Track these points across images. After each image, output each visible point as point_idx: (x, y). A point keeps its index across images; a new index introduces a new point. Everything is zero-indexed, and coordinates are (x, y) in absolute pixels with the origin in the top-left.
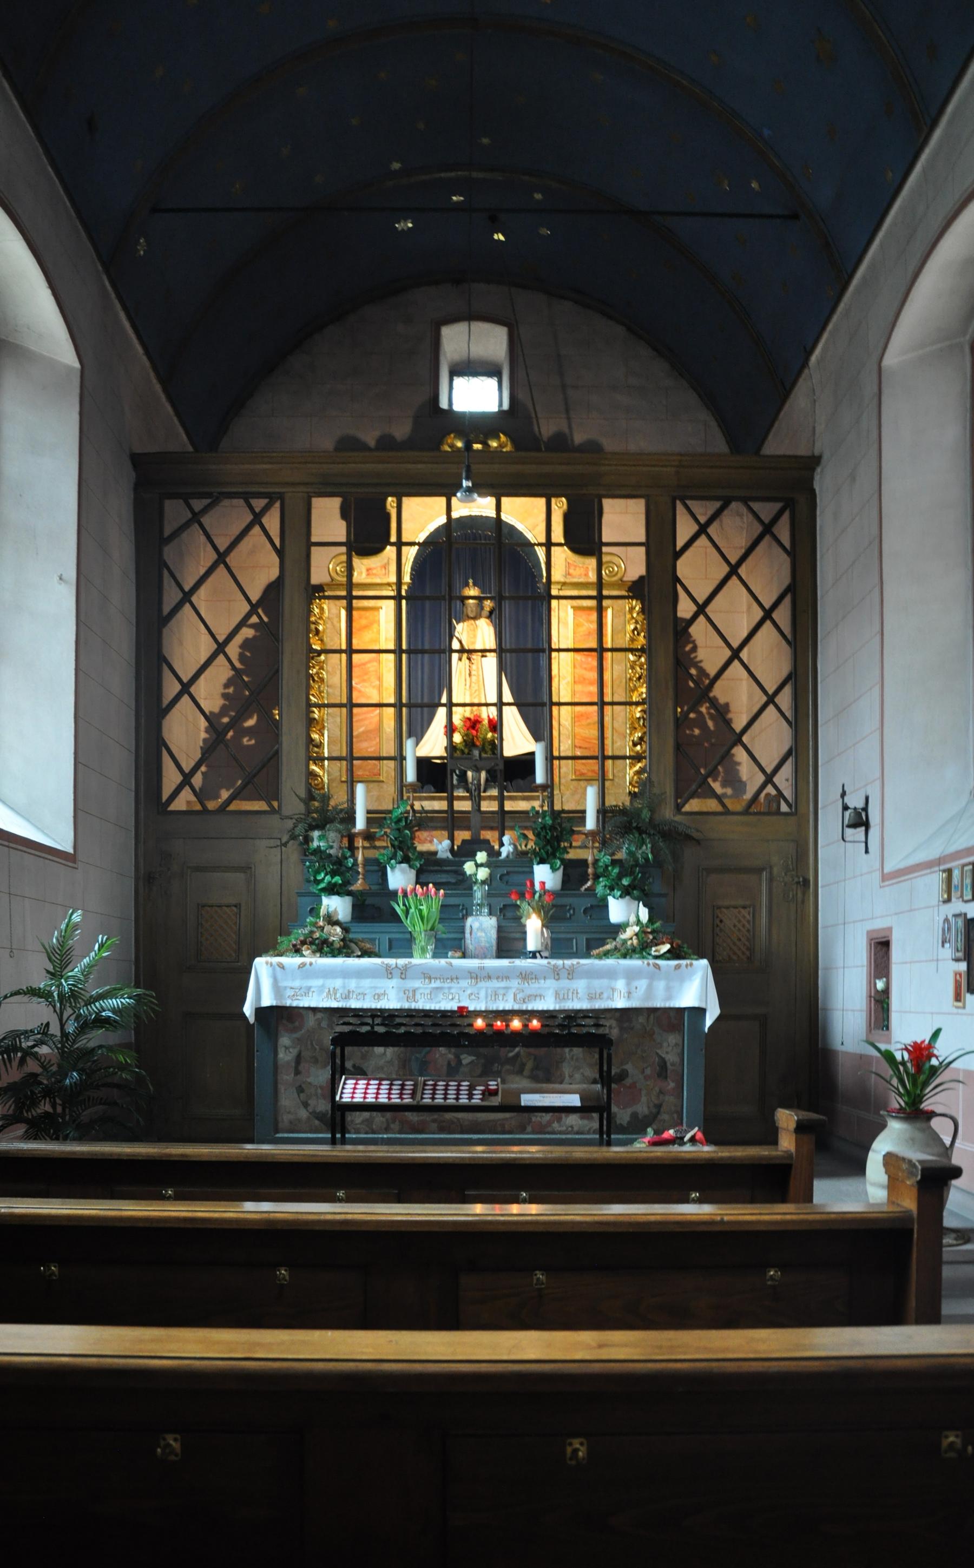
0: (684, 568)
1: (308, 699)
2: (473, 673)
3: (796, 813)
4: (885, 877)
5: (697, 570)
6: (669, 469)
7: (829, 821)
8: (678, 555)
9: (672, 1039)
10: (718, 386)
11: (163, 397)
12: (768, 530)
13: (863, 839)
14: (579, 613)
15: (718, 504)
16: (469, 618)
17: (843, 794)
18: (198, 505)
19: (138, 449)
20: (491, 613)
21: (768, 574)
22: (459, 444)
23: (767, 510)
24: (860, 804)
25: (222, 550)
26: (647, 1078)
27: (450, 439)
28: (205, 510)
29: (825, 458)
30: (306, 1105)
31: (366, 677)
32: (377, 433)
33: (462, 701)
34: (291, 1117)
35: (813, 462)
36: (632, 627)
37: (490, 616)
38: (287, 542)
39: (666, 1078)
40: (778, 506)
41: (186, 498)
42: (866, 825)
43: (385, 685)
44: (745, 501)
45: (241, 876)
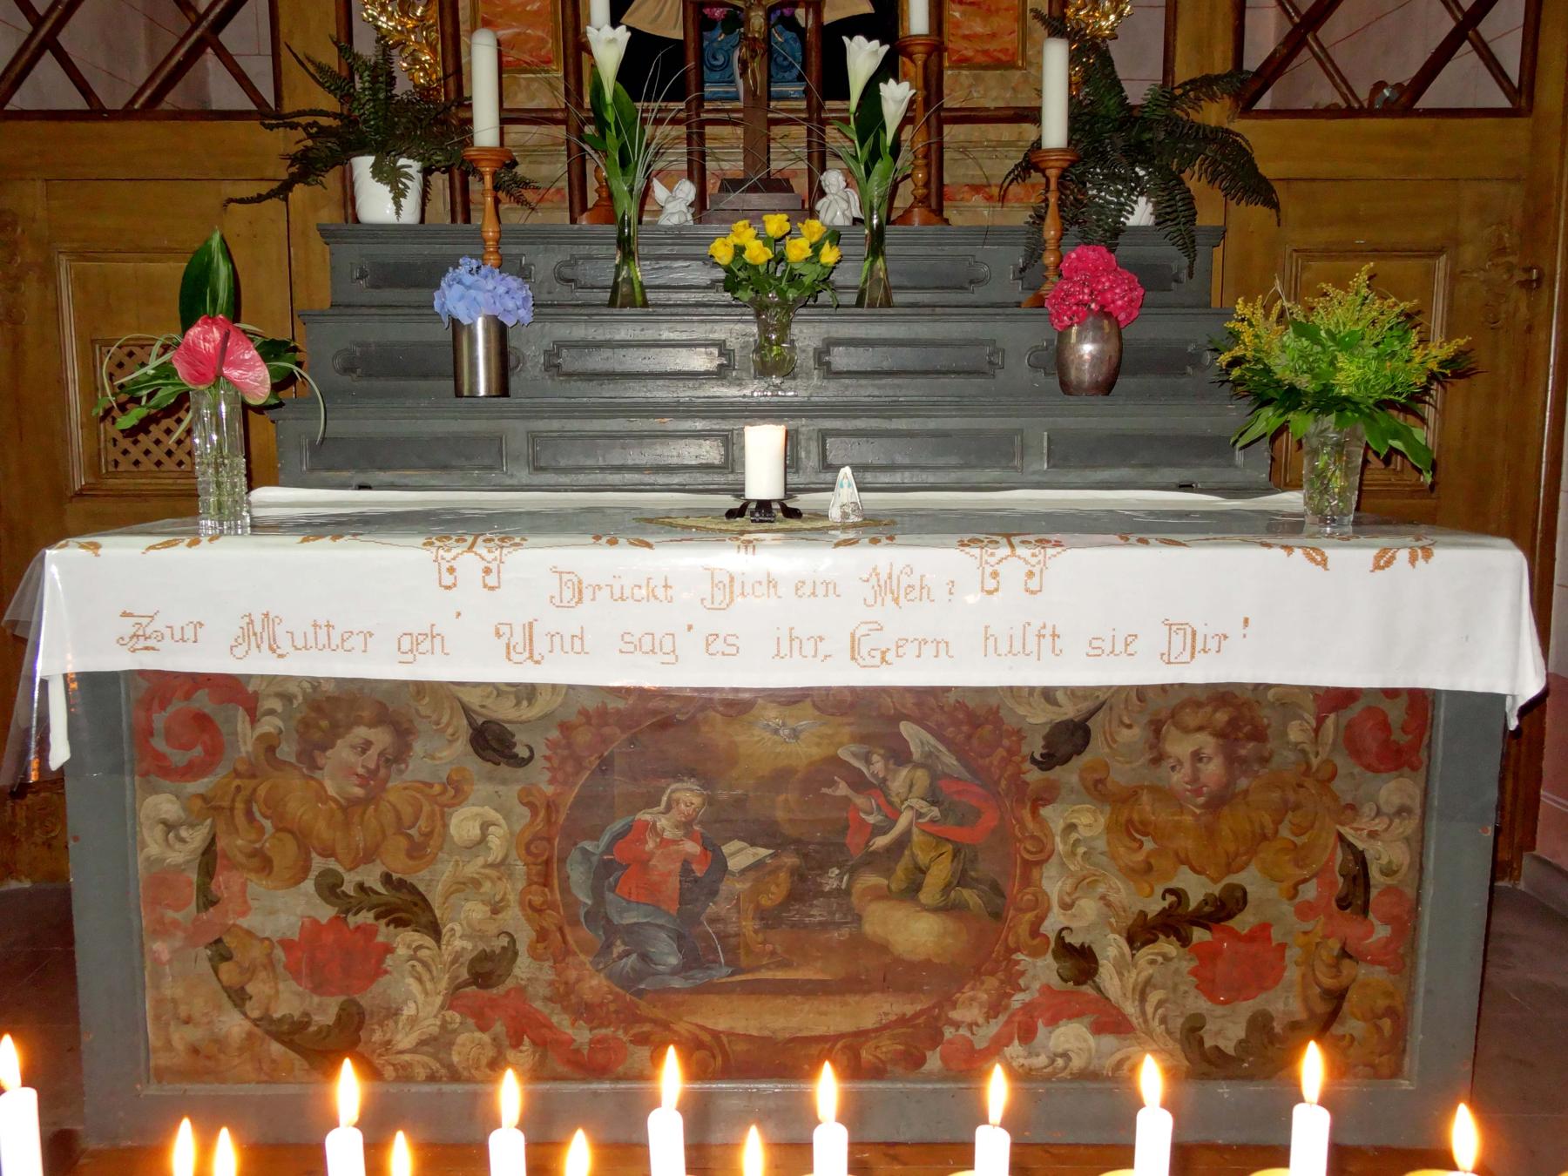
9: (1393, 790)
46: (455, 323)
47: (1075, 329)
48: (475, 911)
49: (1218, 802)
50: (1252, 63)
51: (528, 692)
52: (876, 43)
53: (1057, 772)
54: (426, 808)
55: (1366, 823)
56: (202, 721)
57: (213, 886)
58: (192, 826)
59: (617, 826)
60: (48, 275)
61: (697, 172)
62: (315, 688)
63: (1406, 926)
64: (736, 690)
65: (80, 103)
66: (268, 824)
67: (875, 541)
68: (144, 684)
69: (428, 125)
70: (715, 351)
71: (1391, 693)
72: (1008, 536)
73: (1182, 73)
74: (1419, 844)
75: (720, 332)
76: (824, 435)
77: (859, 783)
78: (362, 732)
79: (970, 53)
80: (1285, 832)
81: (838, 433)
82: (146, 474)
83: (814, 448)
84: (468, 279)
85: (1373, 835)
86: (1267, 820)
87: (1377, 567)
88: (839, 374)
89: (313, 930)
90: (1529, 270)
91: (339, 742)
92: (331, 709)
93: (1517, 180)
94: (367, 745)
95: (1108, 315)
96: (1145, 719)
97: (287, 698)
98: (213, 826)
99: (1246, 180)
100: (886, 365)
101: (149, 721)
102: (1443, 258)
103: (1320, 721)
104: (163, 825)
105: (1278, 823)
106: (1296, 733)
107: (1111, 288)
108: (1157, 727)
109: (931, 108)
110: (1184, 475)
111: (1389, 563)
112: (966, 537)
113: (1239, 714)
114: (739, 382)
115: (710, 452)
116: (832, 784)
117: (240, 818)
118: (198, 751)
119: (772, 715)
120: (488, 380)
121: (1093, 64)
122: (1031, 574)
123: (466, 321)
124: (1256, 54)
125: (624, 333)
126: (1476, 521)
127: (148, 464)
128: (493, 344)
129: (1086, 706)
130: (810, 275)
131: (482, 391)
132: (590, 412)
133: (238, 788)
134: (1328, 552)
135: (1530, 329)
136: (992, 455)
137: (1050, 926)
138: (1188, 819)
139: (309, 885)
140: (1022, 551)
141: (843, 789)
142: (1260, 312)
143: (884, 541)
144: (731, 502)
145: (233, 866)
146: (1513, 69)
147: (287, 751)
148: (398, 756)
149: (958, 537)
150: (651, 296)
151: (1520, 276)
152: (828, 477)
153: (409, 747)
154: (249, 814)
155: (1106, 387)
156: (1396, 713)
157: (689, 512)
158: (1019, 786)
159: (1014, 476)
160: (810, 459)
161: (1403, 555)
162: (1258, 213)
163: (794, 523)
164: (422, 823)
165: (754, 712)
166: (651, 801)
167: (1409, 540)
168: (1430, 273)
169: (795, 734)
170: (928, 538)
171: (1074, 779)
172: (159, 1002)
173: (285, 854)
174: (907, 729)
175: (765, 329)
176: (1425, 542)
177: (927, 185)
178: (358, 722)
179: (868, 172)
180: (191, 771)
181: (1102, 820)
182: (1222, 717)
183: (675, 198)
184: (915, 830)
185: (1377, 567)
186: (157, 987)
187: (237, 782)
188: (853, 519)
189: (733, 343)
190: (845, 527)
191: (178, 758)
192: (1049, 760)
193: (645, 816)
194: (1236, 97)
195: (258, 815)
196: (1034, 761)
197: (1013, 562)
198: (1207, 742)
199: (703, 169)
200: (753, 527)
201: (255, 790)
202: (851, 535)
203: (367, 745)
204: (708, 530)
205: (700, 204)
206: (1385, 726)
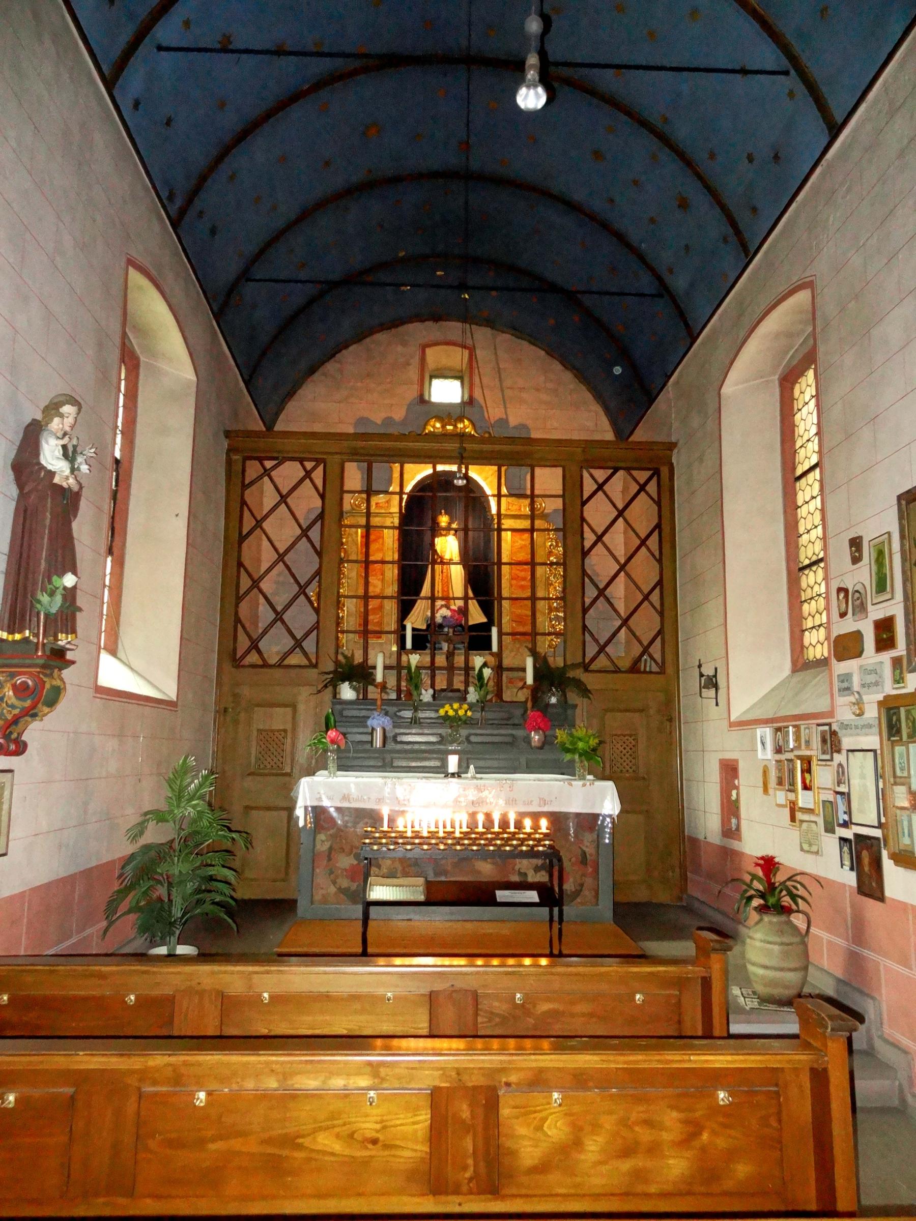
0: (589, 511)
1: (338, 592)
4: (731, 725)
5: (598, 513)
7: (689, 682)
8: (584, 503)
11: (245, 391)
12: (642, 488)
13: (714, 696)
15: (610, 471)
17: (700, 666)
18: (269, 464)
19: (228, 429)
21: (643, 513)
22: (438, 425)
23: (642, 476)
24: (712, 673)
25: (281, 551)
26: (573, 865)
27: (432, 422)
28: (274, 467)
30: (334, 883)
32: (383, 415)
34: (324, 892)
35: (672, 446)
39: (586, 864)
40: (650, 473)
41: (261, 460)
42: (716, 686)
43: (386, 578)
44: (628, 469)
48: (389, 862)
61: (433, 686)
63: (596, 870)
65: (260, 662)
69: (360, 674)
73: (569, 663)
75: (440, 731)
78: (366, 820)
89: (352, 866)
99: (585, 691)
109: (499, 669)
115: (438, 764)
126: (102, 687)
130: (464, 718)
135: (671, 733)
137: (517, 868)
155: (541, 748)
160: (464, 765)
189: (444, 734)
205: (434, 696)
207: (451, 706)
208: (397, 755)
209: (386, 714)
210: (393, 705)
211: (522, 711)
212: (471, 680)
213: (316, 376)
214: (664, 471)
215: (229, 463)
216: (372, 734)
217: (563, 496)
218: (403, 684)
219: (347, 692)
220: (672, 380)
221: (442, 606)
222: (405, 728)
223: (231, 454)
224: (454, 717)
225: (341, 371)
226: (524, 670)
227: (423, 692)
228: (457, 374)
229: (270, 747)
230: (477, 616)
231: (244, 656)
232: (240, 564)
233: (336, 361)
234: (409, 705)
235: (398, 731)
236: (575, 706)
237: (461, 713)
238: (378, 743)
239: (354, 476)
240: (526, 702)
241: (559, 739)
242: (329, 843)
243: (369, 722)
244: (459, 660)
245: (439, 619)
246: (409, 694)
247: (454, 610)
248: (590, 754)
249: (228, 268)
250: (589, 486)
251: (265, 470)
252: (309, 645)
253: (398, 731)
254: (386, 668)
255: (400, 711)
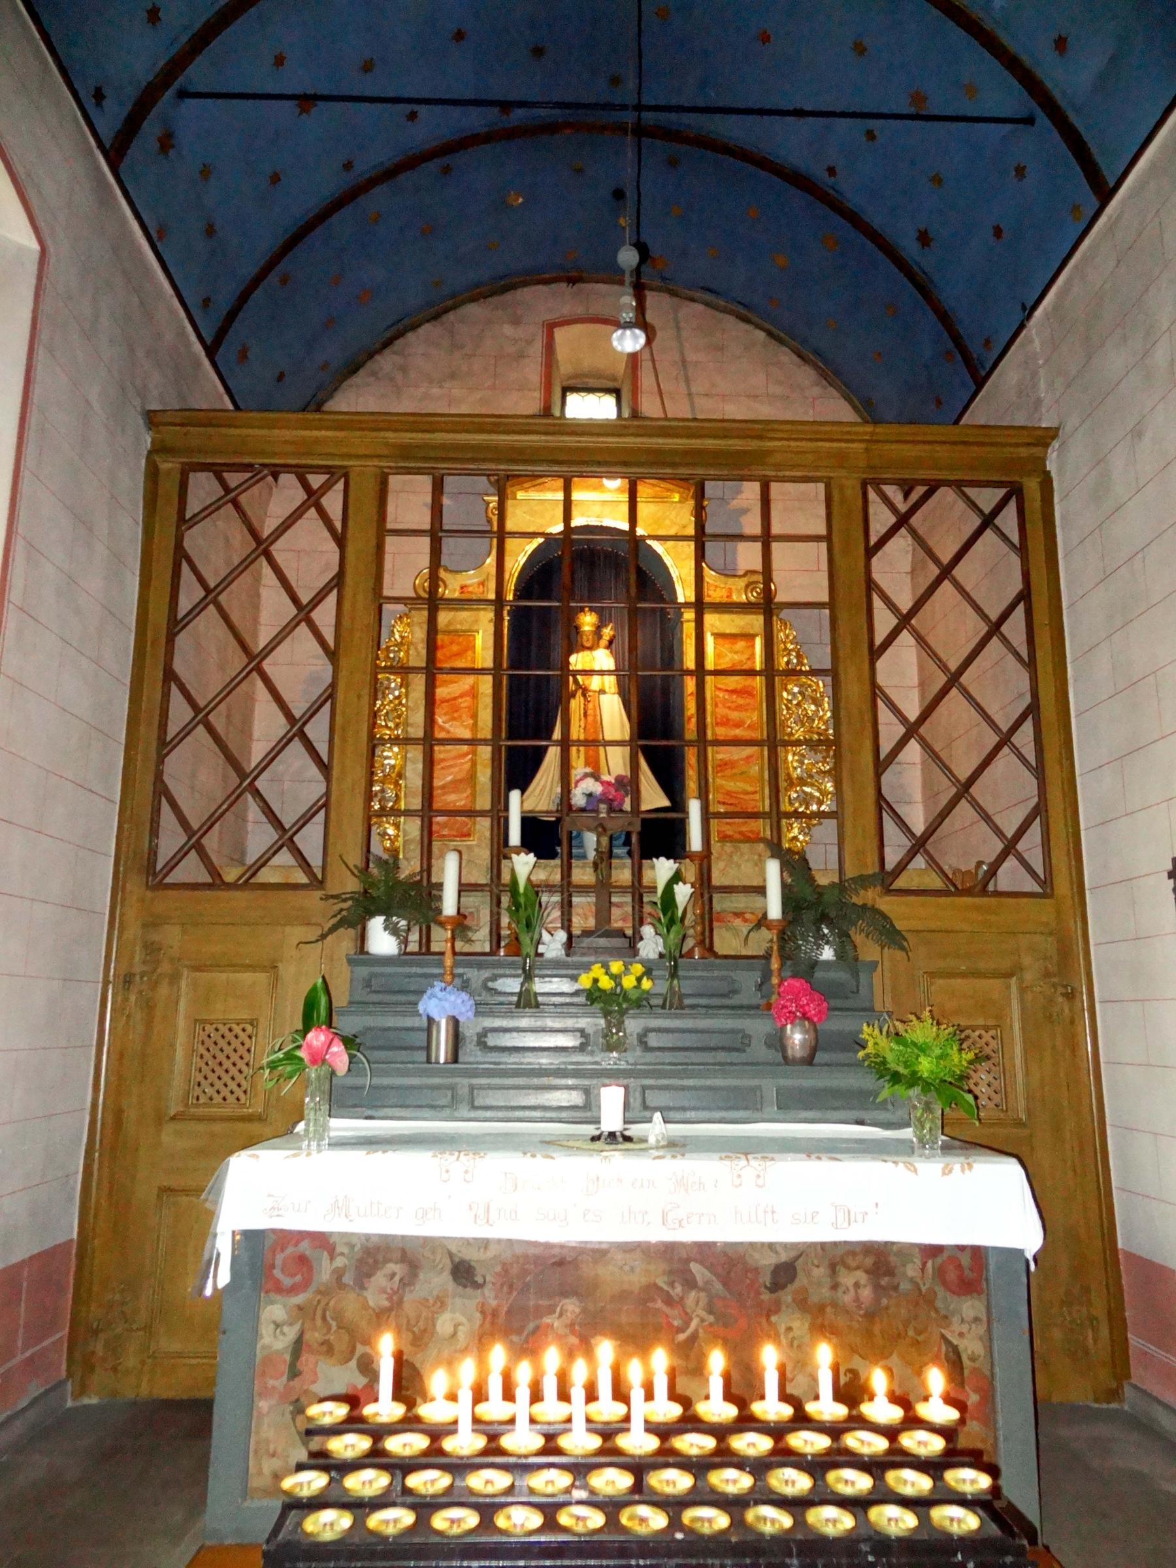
2: (590, 712)
3: (1051, 896)
6: (855, 445)
8: (871, 552)
9: (970, 1307)
10: (919, 344)
12: (988, 521)
14: (720, 641)
16: (584, 648)
20: (611, 642)
21: (992, 572)
23: (987, 498)
28: (244, 487)
29: (1068, 428)
31: (456, 715)
33: (776, 564)
35: (1046, 437)
36: (785, 659)
37: (610, 645)
38: (351, 523)
40: (1001, 492)
41: (217, 471)
43: (480, 723)
44: (958, 485)
45: (262, 977)
46: (430, 1020)
47: (789, 1027)
49: (870, 1316)
50: (889, 866)
51: (485, 1243)
52: (672, 861)
53: (781, 1293)
54: (424, 1314)
55: (956, 1326)
56: (303, 1260)
57: (298, 1364)
58: (291, 1324)
59: (531, 1326)
60: (175, 978)
61: (567, 925)
62: (367, 1241)
64: (600, 1243)
65: (206, 878)
66: (334, 1324)
67: (674, 1157)
68: (273, 1237)
69: (413, 900)
70: (578, 1034)
71: (962, 1248)
72: (746, 1154)
73: (850, 873)
74: (988, 1339)
75: (582, 1023)
76: (644, 1089)
77: (669, 1301)
79: (730, 833)
80: (911, 1333)
81: (651, 1088)
82: (218, 1106)
83: (638, 1095)
84: (440, 995)
85: (961, 1335)
86: (901, 1327)
87: (944, 1174)
88: (652, 1049)
90: (1065, 987)
91: (378, 1273)
92: (374, 1254)
93: (1051, 934)
94: (393, 1275)
95: (808, 1019)
96: (826, 1263)
97: (352, 1246)
98: (303, 1324)
99: (891, 936)
100: (680, 1044)
101: (274, 1259)
102: (1014, 978)
103: (924, 1264)
104: (275, 1325)
105: (906, 1327)
106: (912, 1271)
107: (808, 1004)
108: (833, 1268)
109: (705, 887)
110: (856, 1114)
111: (950, 1172)
112: (723, 1155)
113: (879, 1260)
114: (592, 1053)
115: (576, 1098)
116: (654, 1300)
117: (319, 1322)
118: (298, 1278)
119: (619, 1256)
120: (446, 1053)
121: (796, 865)
122: (758, 1176)
123: (437, 1019)
124: (892, 858)
125: (524, 1022)
127: (218, 1099)
128: (451, 1028)
129: (793, 1254)
130: (634, 995)
131: (442, 1060)
132: (504, 1073)
133: (319, 1302)
134: (916, 1165)
135: (1072, 1022)
136: (743, 1104)
138: (855, 1325)
139: (353, 1363)
140: (754, 1163)
141: (659, 1304)
142: (877, 1031)
143: (679, 1156)
144: (591, 1130)
145: (312, 1351)
146: (1040, 871)
147: (348, 1279)
148: (410, 1280)
149: (719, 1155)
150: (540, 999)
151: (1060, 990)
152: (647, 1114)
153: (416, 1275)
154: (324, 1318)
155: (809, 1060)
156: (966, 1260)
157: (569, 1137)
158: (760, 1304)
159: (757, 1115)
160: (636, 1102)
161: (957, 1167)
162: (892, 955)
163: (628, 1145)
164: (421, 1324)
165: (609, 1255)
166: (551, 1310)
167: (962, 1159)
168: (1008, 987)
169: (632, 1269)
170: (703, 1155)
171: (789, 1299)
172: (258, 1443)
173: (341, 1342)
174: (695, 1267)
175: (609, 1025)
176: (970, 1160)
177: (703, 933)
178: (390, 1261)
179: (668, 931)
180: (293, 1290)
181: (807, 1326)
182: (869, 1261)
183: (554, 940)
184: (701, 1331)
185: (944, 1174)
186: (258, 1433)
187: (319, 1297)
188: (663, 1143)
189: (590, 1031)
190: (657, 1148)
191: (287, 1282)
192: (776, 1286)
193: (547, 1320)
194: (882, 884)
195: (328, 1318)
196: (766, 1287)
197: (750, 1168)
198: (861, 1277)
199: (570, 920)
200: (607, 1147)
201: (328, 1304)
202: (661, 1153)
203: (393, 1275)
204: (583, 1149)
205: (569, 945)
206: (959, 1267)
207: (606, 966)
208: (483, 1081)
209: (465, 986)
210: (480, 966)
211: (757, 977)
212: (647, 909)
213: (357, 379)
214: (1032, 486)
215: (153, 474)
216: (429, 1030)
217: (828, 538)
218: (505, 920)
219: (381, 940)
220: (1038, 313)
221: (586, 775)
222: (509, 1014)
223: (157, 458)
224: (613, 993)
225: (404, 369)
226: (761, 890)
227: (546, 936)
228: (610, 385)
229: (221, 1057)
230: (653, 797)
231: (172, 865)
232: (170, 676)
233: (395, 353)
234: (512, 965)
235: (490, 1023)
236: (873, 965)
237: (629, 982)
238: (442, 1053)
239: (409, 502)
240: (767, 957)
241: (870, 1049)
242: (297, 1327)
243: (421, 1008)
244: (623, 874)
245: (578, 798)
246: (515, 948)
247: (609, 783)
248: (952, 1087)
249: (136, 57)
250: (881, 519)
251: (227, 490)
252: (311, 840)
253: (490, 1023)
254: (464, 888)
255: (494, 978)
